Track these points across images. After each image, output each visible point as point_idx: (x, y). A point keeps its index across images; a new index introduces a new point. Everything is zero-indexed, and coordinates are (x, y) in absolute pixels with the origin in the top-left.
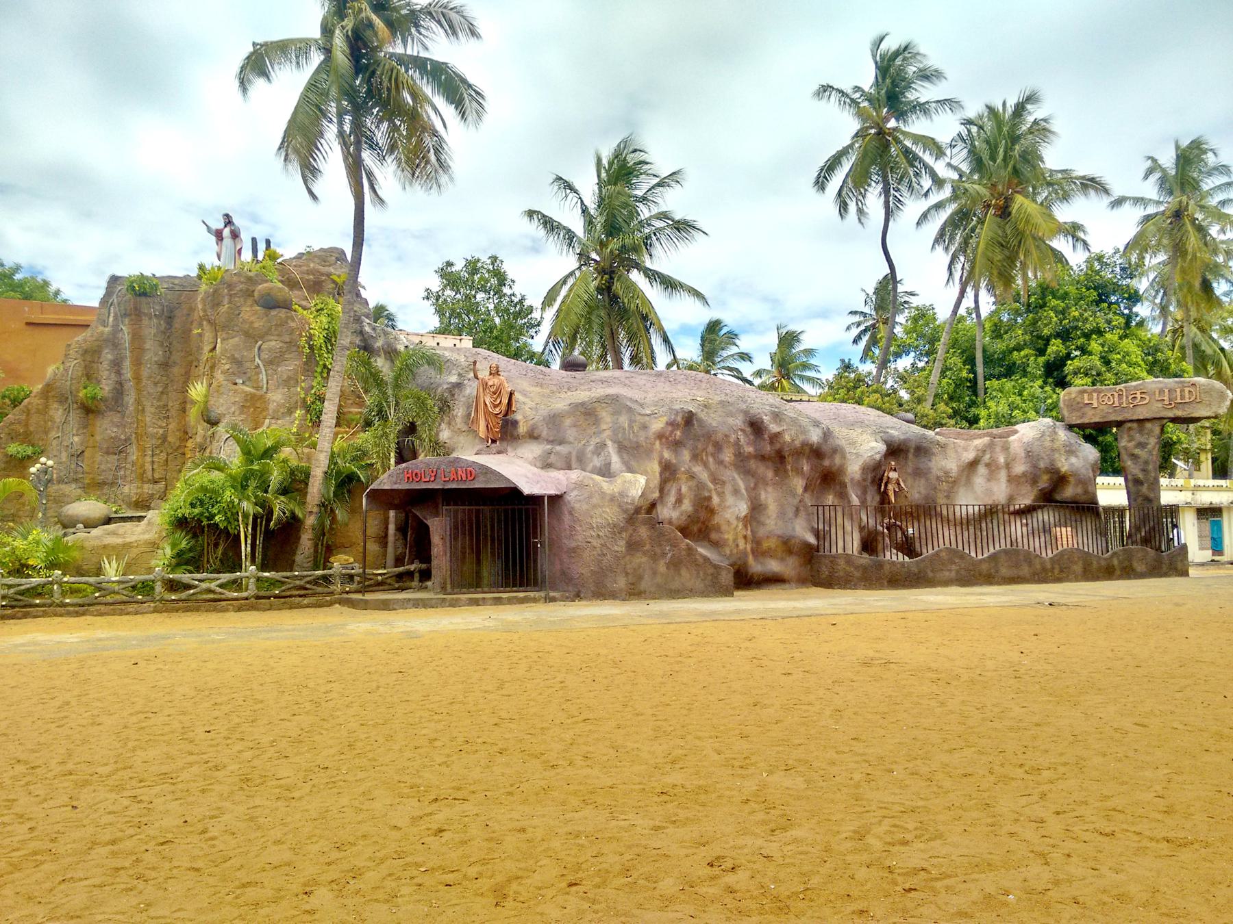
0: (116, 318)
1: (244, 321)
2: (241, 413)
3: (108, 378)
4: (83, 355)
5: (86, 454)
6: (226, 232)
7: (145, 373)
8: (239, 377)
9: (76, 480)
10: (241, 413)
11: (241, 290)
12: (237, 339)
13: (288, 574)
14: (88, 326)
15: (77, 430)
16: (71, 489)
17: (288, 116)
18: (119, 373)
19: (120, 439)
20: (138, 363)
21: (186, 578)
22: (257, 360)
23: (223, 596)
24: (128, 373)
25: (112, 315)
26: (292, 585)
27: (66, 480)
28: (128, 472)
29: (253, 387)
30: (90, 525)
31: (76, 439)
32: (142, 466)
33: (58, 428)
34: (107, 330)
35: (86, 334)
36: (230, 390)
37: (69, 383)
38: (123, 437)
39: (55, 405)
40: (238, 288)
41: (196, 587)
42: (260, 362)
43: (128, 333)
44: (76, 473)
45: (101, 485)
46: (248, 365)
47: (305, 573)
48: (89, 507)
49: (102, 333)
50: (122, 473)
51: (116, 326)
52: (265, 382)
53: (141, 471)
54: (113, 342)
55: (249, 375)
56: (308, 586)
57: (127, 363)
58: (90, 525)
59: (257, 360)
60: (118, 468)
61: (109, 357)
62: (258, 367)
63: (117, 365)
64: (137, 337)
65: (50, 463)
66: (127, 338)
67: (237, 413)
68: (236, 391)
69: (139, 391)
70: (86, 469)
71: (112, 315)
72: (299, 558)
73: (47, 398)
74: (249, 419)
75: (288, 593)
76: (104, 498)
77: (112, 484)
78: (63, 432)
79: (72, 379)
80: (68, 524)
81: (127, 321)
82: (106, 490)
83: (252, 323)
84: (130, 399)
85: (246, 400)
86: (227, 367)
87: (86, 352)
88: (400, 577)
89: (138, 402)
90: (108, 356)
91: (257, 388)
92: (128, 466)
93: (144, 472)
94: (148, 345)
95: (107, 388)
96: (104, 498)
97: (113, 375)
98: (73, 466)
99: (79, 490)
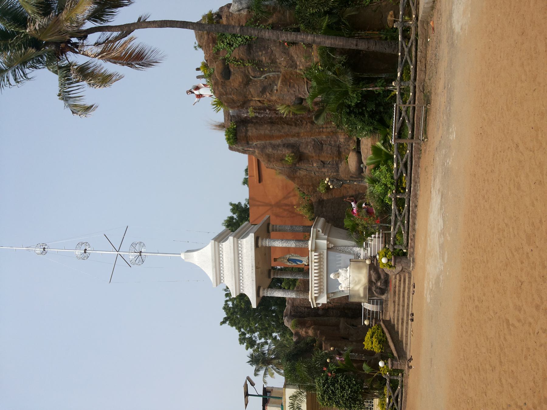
0: (250, 147)
1: (240, 86)
2: (294, 87)
3: (282, 151)
4: (271, 162)
5: (323, 160)
6: (197, 92)
7: (276, 133)
8: (273, 87)
9: (337, 164)
10: (294, 87)
11: (222, 88)
12: (251, 90)
13: (400, 59)
14: (258, 160)
15: (310, 164)
16: (342, 166)
17: (156, 20)
18: (279, 146)
19: (314, 144)
20: (271, 137)
21: (395, 123)
22: (261, 78)
23: (409, 156)
24: (279, 141)
25: (249, 149)
26: (408, 57)
27: (337, 169)
28: (332, 140)
29: (278, 79)
30: (360, 162)
31: (315, 165)
32: (329, 133)
33: (309, 173)
34: (257, 151)
35: (261, 160)
36: (281, 94)
37: (286, 169)
38: (313, 143)
39: (298, 174)
40: (222, 90)
41: (404, 118)
42: (263, 77)
43: (257, 142)
44: (333, 164)
45: (339, 153)
46: (265, 84)
47: (400, 48)
48: (352, 160)
49: (259, 153)
50: (333, 142)
51: (254, 147)
52: (274, 73)
53: (331, 133)
54: (263, 148)
55: (271, 83)
56: (404, 160)
57: (273, 142)
58: (360, 162)
59: (261, 78)
60: (330, 144)
61: (270, 150)
62: (266, 78)
63: (274, 147)
64: (259, 138)
65: (327, 179)
66: (259, 142)
67: (294, 90)
68: (281, 91)
69: (287, 135)
70: (330, 160)
71: (249, 149)
72: (388, 51)
73: (295, 177)
74: (297, 82)
75: (414, 59)
76: (347, 151)
77: (339, 147)
78: (312, 171)
79: (283, 168)
80: (360, 170)
81: (250, 143)
82: (342, 150)
83: (240, 82)
84: (292, 140)
85: (286, 84)
86: (268, 94)
87: (269, 161)
88: (394, 388)
89: (293, 136)
90: (269, 150)
91: (279, 77)
92: (329, 139)
93: (332, 132)
94: (262, 132)
95: (287, 151)
96: (347, 151)
97: (280, 148)
98: (329, 166)
99: (342, 163)
